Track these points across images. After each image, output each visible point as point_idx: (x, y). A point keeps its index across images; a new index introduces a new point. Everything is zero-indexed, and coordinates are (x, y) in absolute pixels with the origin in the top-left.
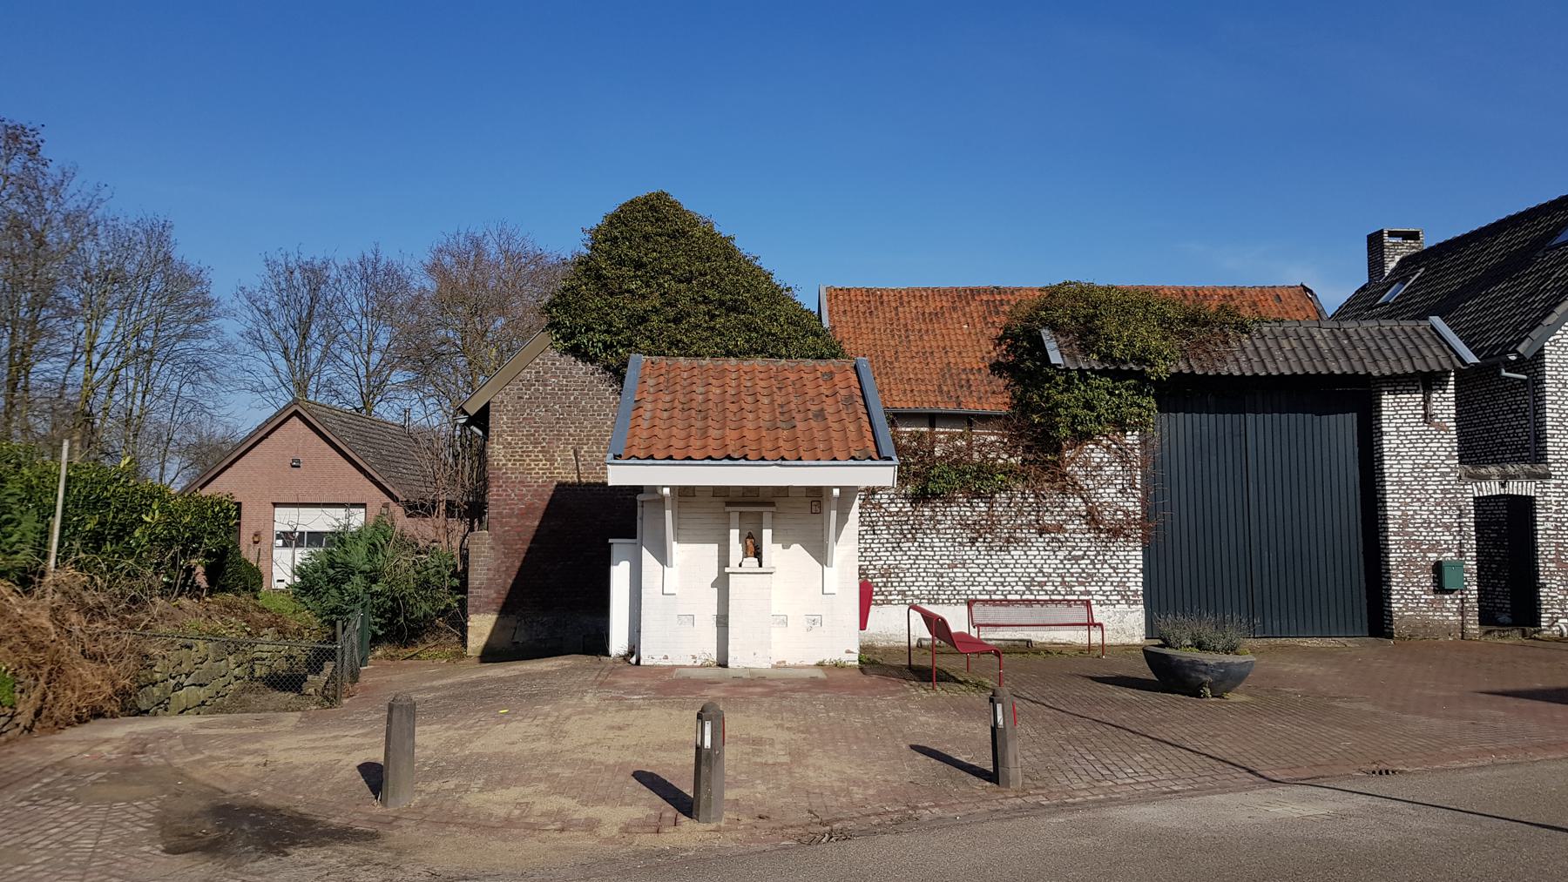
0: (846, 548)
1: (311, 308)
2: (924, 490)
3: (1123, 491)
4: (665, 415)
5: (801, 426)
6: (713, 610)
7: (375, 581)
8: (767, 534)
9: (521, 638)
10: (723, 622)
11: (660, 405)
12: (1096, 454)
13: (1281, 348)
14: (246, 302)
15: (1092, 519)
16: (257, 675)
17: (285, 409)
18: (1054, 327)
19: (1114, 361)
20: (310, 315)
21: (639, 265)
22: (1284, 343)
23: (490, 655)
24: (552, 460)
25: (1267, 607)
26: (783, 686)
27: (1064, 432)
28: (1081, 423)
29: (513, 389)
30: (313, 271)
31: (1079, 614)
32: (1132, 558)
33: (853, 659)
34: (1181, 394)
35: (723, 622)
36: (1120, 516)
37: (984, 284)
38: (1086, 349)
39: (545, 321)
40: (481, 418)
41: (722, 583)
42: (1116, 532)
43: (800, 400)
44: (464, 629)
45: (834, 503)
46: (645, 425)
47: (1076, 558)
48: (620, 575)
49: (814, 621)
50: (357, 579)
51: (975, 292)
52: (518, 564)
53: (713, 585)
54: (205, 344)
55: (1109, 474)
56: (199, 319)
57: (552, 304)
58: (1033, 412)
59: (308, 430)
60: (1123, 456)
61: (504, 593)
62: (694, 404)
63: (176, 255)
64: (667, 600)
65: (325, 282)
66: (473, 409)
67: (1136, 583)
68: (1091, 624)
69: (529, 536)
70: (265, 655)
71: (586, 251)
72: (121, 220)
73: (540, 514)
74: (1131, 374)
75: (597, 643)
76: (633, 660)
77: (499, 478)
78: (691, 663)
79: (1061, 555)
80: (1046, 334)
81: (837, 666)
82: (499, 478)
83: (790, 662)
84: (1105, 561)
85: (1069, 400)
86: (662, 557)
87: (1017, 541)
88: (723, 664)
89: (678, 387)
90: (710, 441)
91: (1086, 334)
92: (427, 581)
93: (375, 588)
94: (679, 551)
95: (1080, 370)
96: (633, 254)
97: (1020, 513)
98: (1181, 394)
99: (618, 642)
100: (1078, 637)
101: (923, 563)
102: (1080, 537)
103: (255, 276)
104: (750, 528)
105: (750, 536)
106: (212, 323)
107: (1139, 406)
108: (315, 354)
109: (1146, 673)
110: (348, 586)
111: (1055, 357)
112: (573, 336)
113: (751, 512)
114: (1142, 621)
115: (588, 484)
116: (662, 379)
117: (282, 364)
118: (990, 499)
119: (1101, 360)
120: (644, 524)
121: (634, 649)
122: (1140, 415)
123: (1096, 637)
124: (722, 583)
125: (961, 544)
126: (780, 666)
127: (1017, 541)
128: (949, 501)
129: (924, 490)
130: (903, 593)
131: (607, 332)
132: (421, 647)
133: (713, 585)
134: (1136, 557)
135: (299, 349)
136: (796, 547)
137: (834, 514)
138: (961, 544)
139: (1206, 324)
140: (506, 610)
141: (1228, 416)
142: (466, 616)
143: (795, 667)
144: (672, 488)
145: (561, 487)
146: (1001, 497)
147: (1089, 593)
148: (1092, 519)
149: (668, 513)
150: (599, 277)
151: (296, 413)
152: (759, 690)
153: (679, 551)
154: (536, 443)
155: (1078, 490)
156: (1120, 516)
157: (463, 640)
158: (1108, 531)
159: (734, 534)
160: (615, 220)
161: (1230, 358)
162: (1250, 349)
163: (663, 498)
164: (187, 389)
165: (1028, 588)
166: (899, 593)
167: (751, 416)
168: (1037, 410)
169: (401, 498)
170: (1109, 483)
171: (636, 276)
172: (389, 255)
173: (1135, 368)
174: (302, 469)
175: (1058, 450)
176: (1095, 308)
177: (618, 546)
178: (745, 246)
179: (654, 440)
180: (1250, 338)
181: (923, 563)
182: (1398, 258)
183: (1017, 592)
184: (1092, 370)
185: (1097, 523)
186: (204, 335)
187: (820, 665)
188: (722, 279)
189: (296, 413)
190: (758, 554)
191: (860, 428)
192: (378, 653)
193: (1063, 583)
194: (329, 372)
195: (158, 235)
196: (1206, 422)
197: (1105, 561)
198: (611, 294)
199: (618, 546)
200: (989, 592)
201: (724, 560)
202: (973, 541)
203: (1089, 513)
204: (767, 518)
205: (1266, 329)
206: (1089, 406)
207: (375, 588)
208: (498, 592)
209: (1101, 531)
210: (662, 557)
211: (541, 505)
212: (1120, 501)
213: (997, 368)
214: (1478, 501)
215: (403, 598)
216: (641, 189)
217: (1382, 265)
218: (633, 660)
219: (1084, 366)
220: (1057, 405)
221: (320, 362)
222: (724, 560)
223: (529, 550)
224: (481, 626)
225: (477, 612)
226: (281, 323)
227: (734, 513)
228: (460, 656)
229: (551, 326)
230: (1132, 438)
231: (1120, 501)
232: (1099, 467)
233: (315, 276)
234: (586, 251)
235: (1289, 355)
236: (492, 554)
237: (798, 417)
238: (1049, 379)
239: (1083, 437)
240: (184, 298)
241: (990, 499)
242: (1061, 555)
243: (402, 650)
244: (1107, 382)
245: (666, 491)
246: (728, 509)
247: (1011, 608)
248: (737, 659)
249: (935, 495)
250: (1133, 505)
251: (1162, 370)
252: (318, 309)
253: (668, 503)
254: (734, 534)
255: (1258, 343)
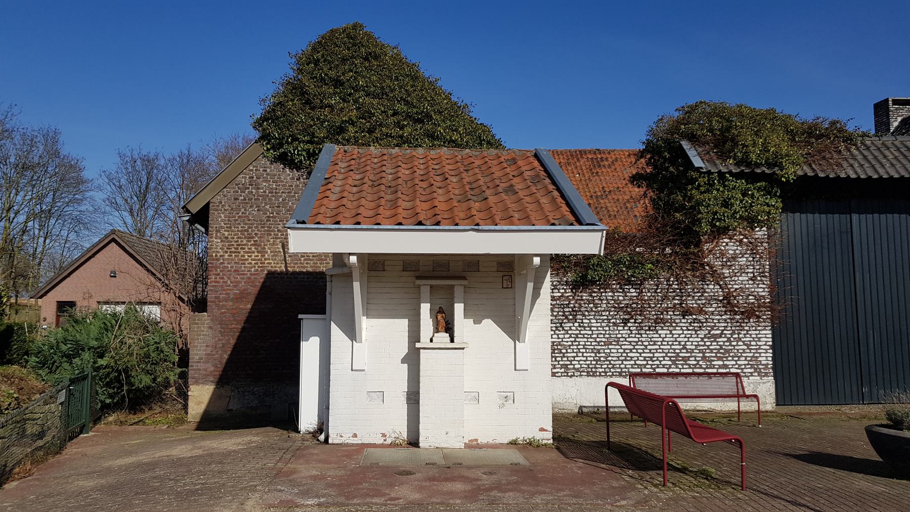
0: (539, 319)
1: (148, 184)
2: (584, 277)
3: (753, 279)
4: (355, 189)
5: (492, 200)
6: (403, 386)
7: (101, 356)
8: (459, 308)
9: (235, 405)
10: (413, 398)
11: (350, 181)
12: (729, 246)
13: (885, 157)
14: (107, 180)
15: (728, 302)
16: (29, 432)
17: (106, 236)
18: (693, 138)
19: (749, 164)
20: (147, 187)
21: (337, 83)
22: (887, 153)
23: (211, 422)
24: (263, 252)
25: (873, 377)
26: (486, 480)
27: (706, 228)
28: (719, 220)
29: (230, 192)
30: (149, 161)
31: (728, 386)
32: (761, 338)
33: (547, 437)
34: (803, 195)
35: (413, 398)
36: (752, 299)
37: (589, 148)
38: (723, 156)
39: (256, 135)
40: (202, 217)
41: (413, 359)
42: (750, 313)
43: (488, 179)
44: (185, 397)
45: (531, 275)
46: (333, 197)
47: (715, 337)
48: (309, 349)
49: (508, 398)
50: (86, 355)
51: (582, 153)
52: (233, 342)
53: (403, 361)
54: (83, 208)
55: (742, 264)
56: (80, 192)
57: (264, 119)
58: (677, 210)
59: (122, 252)
60: (753, 248)
61: (221, 367)
62: (383, 181)
63: (64, 152)
64: (356, 379)
65: (157, 168)
66: (195, 208)
67: (766, 358)
68: (740, 396)
69: (243, 316)
70: (36, 416)
71: (291, 74)
72: (30, 129)
73: (252, 298)
74: (763, 177)
75: (290, 421)
76: (322, 437)
77: (217, 267)
78: (380, 441)
79: (702, 333)
80: (685, 145)
81: (530, 445)
82: (217, 267)
83: (482, 440)
84: (739, 339)
85: (710, 201)
86: (352, 333)
87: (664, 321)
88: (414, 442)
89: (368, 168)
90: (400, 210)
91: (723, 142)
92: (147, 356)
93: (102, 362)
94: (367, 325)
95: (720, 172)
96: (332, 73)
97: (665, 298)
98: (803, 195)
99: (308, 419)
100: (730, 406)
101: (582, 341)
102: (719, 321)
103: (112, 164)
104: (441, 303)
105: (441, 311)
106: (88, 194)
107: (768, 205)
108: (150, 213)
109: (872, 455)
110: (77, 361)
111: (697, 162)
112: (281, 145)
113: (439, 286)
114: (773, 390)
115: (294, 273)
116: (353, 162)
117: (129, 220)
118: (639, 285)
119: (737, 164)
120: (333, 301)
121: (322, 427)
122: (769, 213)
123: (747, 406)
124: (413, 359)
125: (615, 324)
126: (473, 445)
127: (664, 321)
128: (606, 286)
129: (584, 277)
130: (565, 366)
131: (308, 142)
132: (147, 414)
133: (403, 361)
134: (766, 335)
135: (140, 210)
136: (488, 323)
137: (530, 286)
138: (615, 324)
139: (821, 136)
140: (223, 381)
141: (836, 216)
142: (187, 387)
143: (488, 446)
144: (360, 256)
145: (271, 275)
146: (650, 284)
147: (726, 366)
148: (728, 302)
149: (356, 286)
150: (303, 94)
151: (113, 240)
152: (459, 486)
153: (367, 325)
154: (250, 238)
155: (717, 277)
156: (752, 299)
157: (185, 407)
158: (742, 313)
159: (425, 308)
160: (321, 45)
161: (845, 164)
162: (860, 157)
163: (350, 267)
164: (72, 236)
165: (674, 362)
166: (563, 366)
167: (440, 191)
168: (681, 208)
169: (186, 299)
170: (742, 271)
171: (335, 94)
172: (196, 152)
173: (767, 171)
174: (117, 279)
175: (698, 244)
176: (728, 121)
177: (308, 321)
178: (427, 70)
179: (341, 209)
180: (858, 149)
181: (582, 341)
182: (899, 119)
183: (664, 366)
184: (730, 173)
185: (733, 306)
186: (79, 202)
187: (514, 443)
188: (409, 95)
189: (113, 240)
190: (449, 329)
191: (554, 200)
192: (111, 419)
193: (704, 358)
194: (158, 223)
195: (52, 139)
196: (819, 221)
197: (739, 339)
198: (313, 109)
199: (308, 321)
200: (639, 366)
201: (414, 335)
202: (625, 322)
203: (725, 298)
204: (458, 291)
205: (868, 143)
206: (726, 204)
207: (102, 362)
208: (215, 366)
209: (736, 313)
210: (352, 333)
211: (254, 291)
212: (749, 285)
213: (636, 179)
214: (325, 313)
215: (126, 370)
216: (342, 22)
217: (888, 124)
218: (322, 437)
219: (724, 170)
220: (699, 203)
221: (153, 216)
222: (414, 335)
223: (243, 329)
224: (200, 396)
225: (197, 383)
226: (127, 195)
227: (425, 286)
228: (181, 421)
229: (262, 138)
230: (760, 233)
231: (749, 285)
232: (734, 258)
233: (150, 163)
234: (291, 74)
235: (894, 162)
236: (210, 332)
237: (488, 192)
238: (692, 181)
239: (719, 232)
240: (70, 179)
241: (639, 285)
242: (702, 333)
243: (132, 416)
244: (741, 183)
245: (353, 259)
246: (418, 282)
247: (659, 380)
248: (429, 438)
249: (593, 282)
250: (762, 290)
251: (791, 172)
252: (152, 185)
253: (356, 274)
254: (425, 308)
255: (866, 153)
